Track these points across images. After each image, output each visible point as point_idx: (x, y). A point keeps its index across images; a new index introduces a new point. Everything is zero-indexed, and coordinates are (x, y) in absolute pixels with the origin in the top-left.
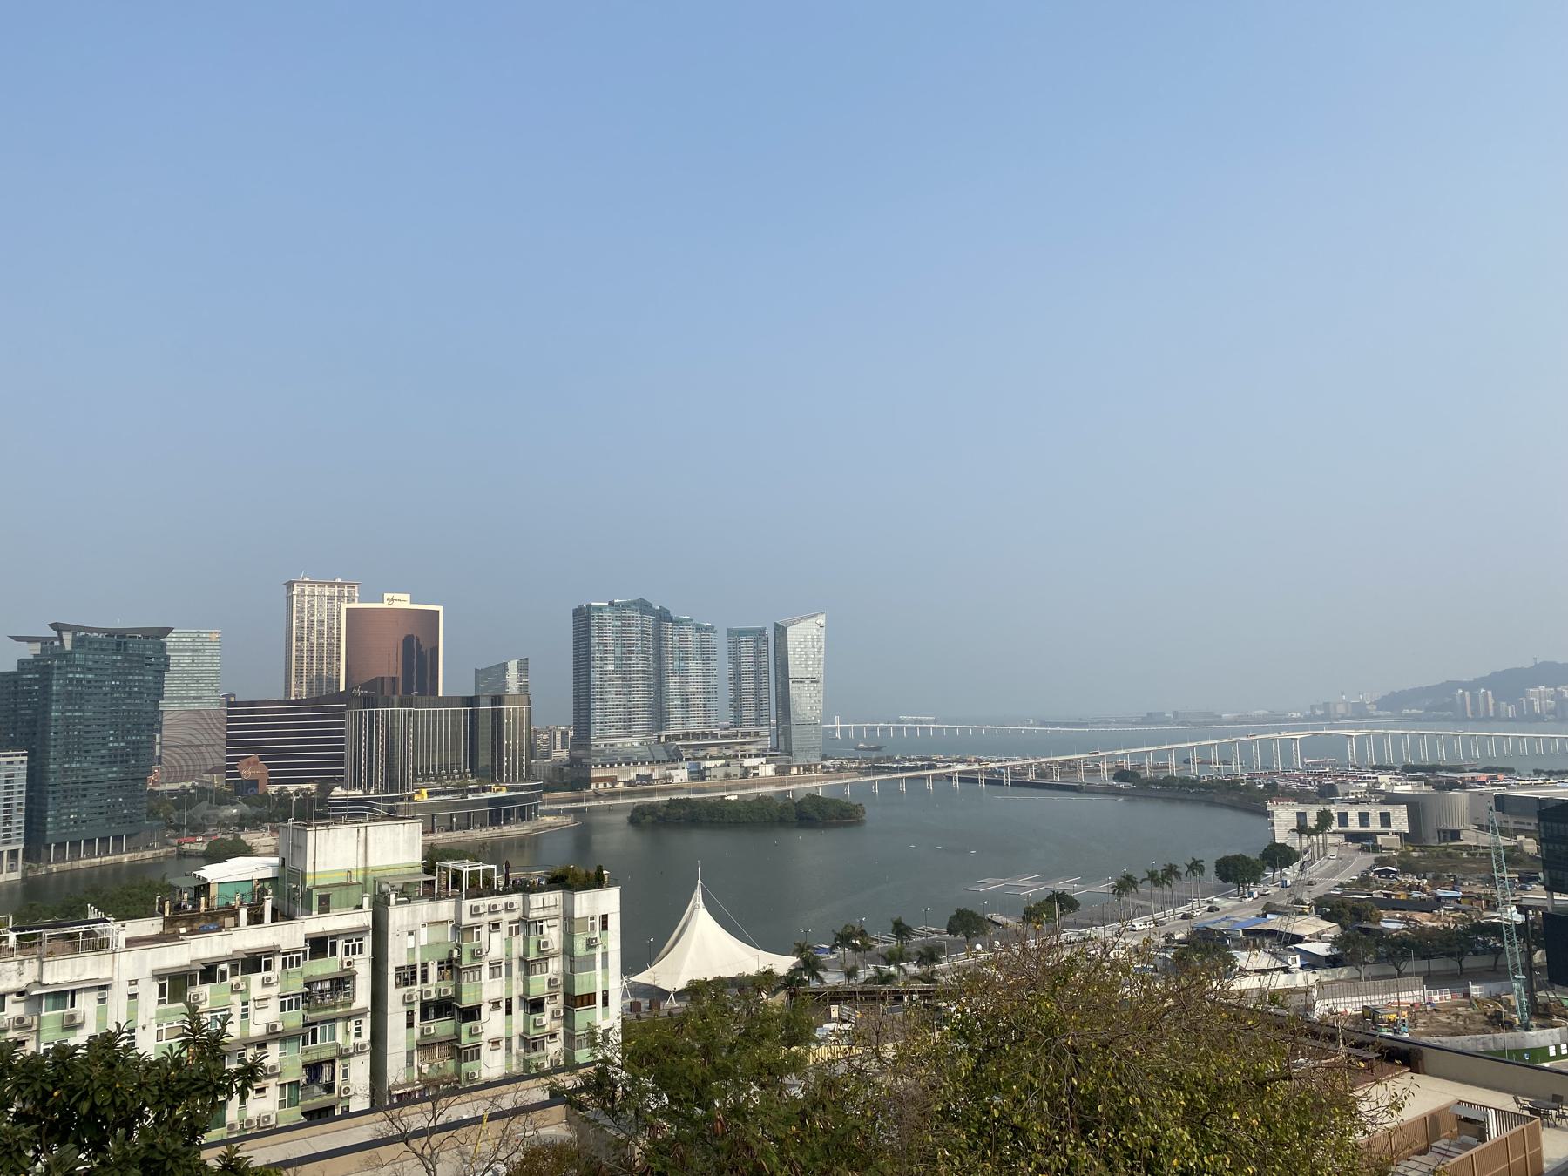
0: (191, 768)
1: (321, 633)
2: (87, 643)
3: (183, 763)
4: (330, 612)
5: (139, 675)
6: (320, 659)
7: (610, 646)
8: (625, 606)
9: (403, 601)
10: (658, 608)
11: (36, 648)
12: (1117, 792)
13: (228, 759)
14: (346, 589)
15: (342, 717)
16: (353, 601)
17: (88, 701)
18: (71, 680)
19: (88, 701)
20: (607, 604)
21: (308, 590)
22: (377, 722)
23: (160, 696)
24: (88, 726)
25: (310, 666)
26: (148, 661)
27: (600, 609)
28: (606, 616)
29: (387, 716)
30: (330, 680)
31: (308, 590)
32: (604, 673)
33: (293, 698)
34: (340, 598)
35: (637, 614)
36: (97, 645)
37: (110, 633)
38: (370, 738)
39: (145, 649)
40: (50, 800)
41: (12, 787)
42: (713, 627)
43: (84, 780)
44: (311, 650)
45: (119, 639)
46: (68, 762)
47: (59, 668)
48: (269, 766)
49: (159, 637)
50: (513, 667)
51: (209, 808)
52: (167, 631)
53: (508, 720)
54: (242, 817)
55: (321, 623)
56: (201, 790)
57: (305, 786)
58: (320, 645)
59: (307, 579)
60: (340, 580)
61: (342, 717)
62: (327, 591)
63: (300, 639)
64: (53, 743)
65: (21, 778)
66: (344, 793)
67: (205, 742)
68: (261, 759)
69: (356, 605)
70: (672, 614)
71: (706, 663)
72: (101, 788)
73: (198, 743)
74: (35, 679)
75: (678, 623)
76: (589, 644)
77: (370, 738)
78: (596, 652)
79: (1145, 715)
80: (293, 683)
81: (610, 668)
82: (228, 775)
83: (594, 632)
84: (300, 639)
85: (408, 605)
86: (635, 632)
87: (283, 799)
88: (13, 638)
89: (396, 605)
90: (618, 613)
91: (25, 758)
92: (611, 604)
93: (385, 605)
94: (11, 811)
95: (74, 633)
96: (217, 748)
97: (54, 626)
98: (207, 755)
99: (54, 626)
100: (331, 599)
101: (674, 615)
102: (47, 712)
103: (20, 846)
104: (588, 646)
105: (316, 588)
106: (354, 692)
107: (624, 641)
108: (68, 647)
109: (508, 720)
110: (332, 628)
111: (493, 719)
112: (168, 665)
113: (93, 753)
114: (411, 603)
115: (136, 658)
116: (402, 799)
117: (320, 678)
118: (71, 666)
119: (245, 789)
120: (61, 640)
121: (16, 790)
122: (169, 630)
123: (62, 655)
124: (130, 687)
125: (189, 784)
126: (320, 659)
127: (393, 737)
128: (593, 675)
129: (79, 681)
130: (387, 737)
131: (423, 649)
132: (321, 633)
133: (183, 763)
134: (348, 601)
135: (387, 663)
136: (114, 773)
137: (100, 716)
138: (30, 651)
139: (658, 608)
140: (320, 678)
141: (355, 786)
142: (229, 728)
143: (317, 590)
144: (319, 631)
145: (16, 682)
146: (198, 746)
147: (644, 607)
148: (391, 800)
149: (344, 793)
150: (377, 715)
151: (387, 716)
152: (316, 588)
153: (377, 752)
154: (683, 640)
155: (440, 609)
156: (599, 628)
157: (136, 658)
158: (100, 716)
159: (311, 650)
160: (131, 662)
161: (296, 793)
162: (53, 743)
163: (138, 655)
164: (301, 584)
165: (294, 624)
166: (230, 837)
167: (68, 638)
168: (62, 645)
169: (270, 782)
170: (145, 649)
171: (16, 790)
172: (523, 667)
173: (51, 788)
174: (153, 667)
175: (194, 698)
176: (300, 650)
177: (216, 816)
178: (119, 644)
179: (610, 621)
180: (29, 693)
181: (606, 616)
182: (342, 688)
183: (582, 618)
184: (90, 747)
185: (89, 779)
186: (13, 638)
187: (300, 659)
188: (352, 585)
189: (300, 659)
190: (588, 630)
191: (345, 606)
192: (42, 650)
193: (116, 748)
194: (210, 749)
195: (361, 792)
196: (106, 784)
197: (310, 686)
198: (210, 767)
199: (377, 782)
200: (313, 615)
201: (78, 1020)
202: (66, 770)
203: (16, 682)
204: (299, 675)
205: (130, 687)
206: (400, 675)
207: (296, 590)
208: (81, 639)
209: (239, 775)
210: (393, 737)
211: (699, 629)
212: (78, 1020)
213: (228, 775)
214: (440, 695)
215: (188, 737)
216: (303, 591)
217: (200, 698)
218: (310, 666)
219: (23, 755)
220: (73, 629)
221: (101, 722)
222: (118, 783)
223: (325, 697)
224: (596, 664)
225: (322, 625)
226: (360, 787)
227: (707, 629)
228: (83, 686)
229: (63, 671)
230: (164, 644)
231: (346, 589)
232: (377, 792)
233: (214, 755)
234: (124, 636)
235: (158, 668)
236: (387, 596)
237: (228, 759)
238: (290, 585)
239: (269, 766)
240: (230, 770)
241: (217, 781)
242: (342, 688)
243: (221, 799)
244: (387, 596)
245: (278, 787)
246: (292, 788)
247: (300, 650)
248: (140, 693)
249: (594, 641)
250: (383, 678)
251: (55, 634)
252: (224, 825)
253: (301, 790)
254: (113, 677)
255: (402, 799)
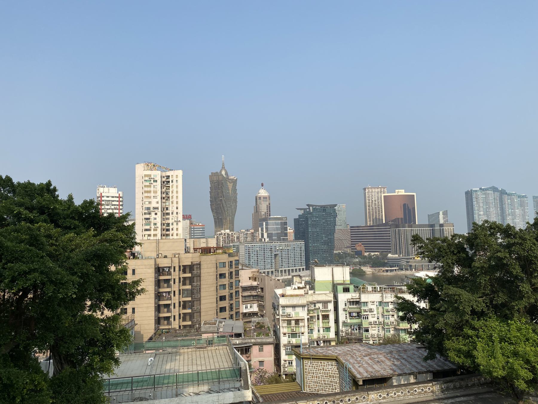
0: (340, 246)
1: (375, 204)
2: (316, 210)
3: (338, 245)
4: (378, 197)
5: (330, 218)
6: (376, 212)
7: (481, 205)
8: (487, 189)
9: (402, 192)
10: (501, 189)
11: (302, 212)
12: (287, 382)
13: (352, 244)
14: (382, 189)
15: (389, 231)
16: (385, 193)
17: (317, 226)
18: (313, 220)
19: (317, 226)
20: (479, 189)
21: (370, 190)
22: (401, 233)
23: (335, 225)
24: (318, 234)
25: (373, 214)
26: (331, 214)
27: (476, 191)
28: (479, 193)
29: (404, 231)
30: (379, 219)
31: (370, 190)
32: (479, 215)
33: (368, 225)
34: (381, 192)
35: (492, 192)
36: (318, 210)
37: (321, 206)
38: (399, 238)
39: (330, 211)
40: (310, 254)
41: (301, 251)
42: (526, 196)
43: (318, 249)
44: (373, 210)
45: (324, 208)
46: (314, 244)
47: (310, 217)
48: (365, 246)
49: (333, 207)
50: (441, 213)
51: (350, 259)
52: (336, 205)
53: (446, 232)
54: (360, 262)
55: (375, 201)
56: (344, 253)
57: (376, 253)
58: (376, 208)
59: (370, 187)
60: (380, 187)
61: (389, 231)
62: (376, 190)
63: (369, 206)
64: (310, 238)
65: (303, 248)
66: (392, 256)
67: (344, 239)
68: (362, 244)
69: (386, 194)
70: (506, 191)
71: (524, 210)
72: (323, 252)
73: (342, 239)
74: (304, 220)
75: (509, 195)
76: (473, 204)
77: (399, 238)
78: (476, 207)
79: (297, 217)
80: (368, 220)
81: (482, 213)
82: (352, 249)
83: (474, 200)
84: (369, 206)
85: (404, 193)
86: (491, 199)
87: (370, 257)
88: (298, 209)
89: (400, 194)
90: (484, 192)
91: (304, 243)
92: (481, 189)
93: (396, 194)
94: (250, 259)
95: (313, 207)
96: (347, 240)
97: (308, 205)
98: (344, 243)
99: (308, 205)
100: (378, 193)
101: (508, 192)
102: (308, 229)
103: (305, 267)
104: (472, 205)
105: (373, 190)
106: (389, 223)
107: (486, 202)
108: (311, 211)
109: (446, 232)
110: (379, 202)
111: (440, 232)
112: (337, 216)
113: (320, 241)
114: (405, 192)
115: (328, 214)
116: (411, 259)
117: (376, 219)
118: (313, 216)
119: (359, 254)
120: (309, 209)
121: (302, 251)
122: (336, 205)
123: (309, 213)
124: (328, 222)
125: (340, 251)
126: (376, 212)
127: (407, 238)
128: (475, 216)
129: (315, 220)
130: (405, 238)
131: (410, 208)
132: (375, 204)
133: (338, 245)
134: (383, 193)
135: (399, 214)
136: (325, 247)
137: (321, 231)
138: (302, 212)
139: (501, 189)
140: (376, 219)
141: (395, 254)
142: (351, 234)
143: (373, 190)
144: (375, 203)
145: (298, 221)
146: (342, 240)
147: (495, 189)
148: (407, 259)
149: (392, 256)
150: (401, 231)
151: (404, 231)
152: (373, 190)
153: (402, 243)
154: (512, 202)
155: (415, 194)
156: (476, 198)
157: (328, 214)
158: (321, 231)
159: (373, 210)
160: (327, 215)
161: (373, 256)
162: (310, 238)
163: (329, 213)
164: (368, 188)
165: (367, 202)
166: (358, 268)
167: (311, 208)
168: (310, 210)
169: (365, 252)
170: (330, 211)
171: (302, 251)
172: (445, 213)
173: (310, 251)
174: (333, 216)
175: (340, 225)
176: (369, 210)
177: (352, 261)
178: (324, 210)
179: (481, 196)
180: (302, 224)
181: (479, 193)
182: (384, 222)
183: (469, 195)
184: (319, 240)
185: (319, 249)
186: (298, 209)
187: (369, 212)
188: (384, 188)
189: (369, 212)
190: (472, 199)
191: (383, 195)
192: (304, 212)
193: (325, 240)
194: (345, 241)
195: (397, 256)
196: (324, 250)
197: (373, 221)
198: (346, 246)
199: (402, 253)
200: (373, 198)
201: (373, 310)
202: (314, 246)
203: (298, 221)
204: (370, 218)
205: (328, 222)
206: (403, 217)
207: (367, 190)
208: (314, 209)
209: (356, 249)
210: (407, 238)
211: (519, 197)
212: (373, 310)
213: (352, 249)
214: (417, 224)
215: (339, 237)
216: (369, 191)
217: (341, 225)
218: (373, 214)
219: (303, 242)
220: (312, 206)
221: (321, 232)
222: (327, 250)
223: (378, 224)
224: (476, 212)
225: (376, 201)
226: (397, 254)
227: (523, 197)
228: (316, 222)
229: (311, 218)
230: (335, 209)
231: (382, 189)
232: (403, 256)
233: (346, 242)
234: (325, 207)
235: (334, 216)
236: (397, 191)
237: (352, 244)
238: (365, 189)
239: (365, 246)
240: (352, 247)
241: (349, 251)
242: (384, 222)
243: (353, 257)
244: (397, 191)
245: (368, 253)
246: (372, 254)
247: (369, 210)
248: (330, 224)
249: (475, 203)
250: (398, 218)
251: (308, 207)
252: (355, 264)
253: (375, 254)
254: (323, 219)
255: (411, 259)
